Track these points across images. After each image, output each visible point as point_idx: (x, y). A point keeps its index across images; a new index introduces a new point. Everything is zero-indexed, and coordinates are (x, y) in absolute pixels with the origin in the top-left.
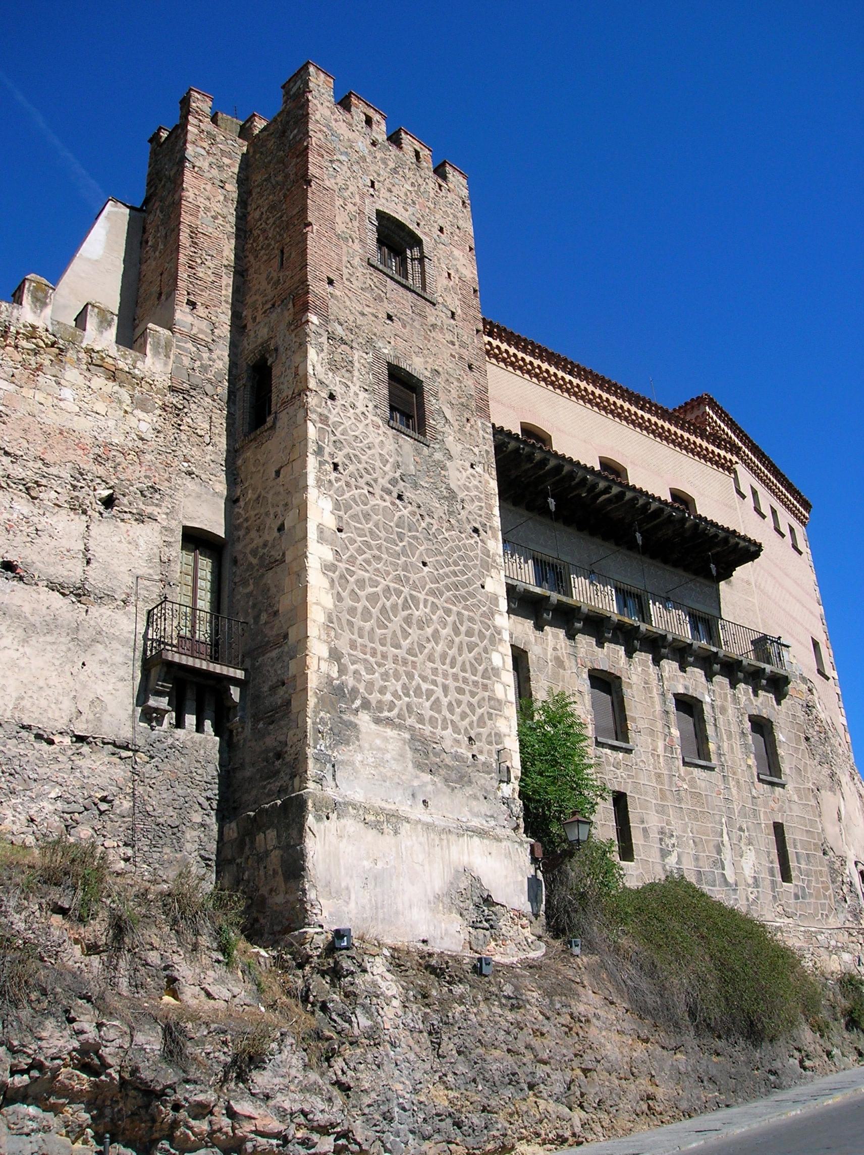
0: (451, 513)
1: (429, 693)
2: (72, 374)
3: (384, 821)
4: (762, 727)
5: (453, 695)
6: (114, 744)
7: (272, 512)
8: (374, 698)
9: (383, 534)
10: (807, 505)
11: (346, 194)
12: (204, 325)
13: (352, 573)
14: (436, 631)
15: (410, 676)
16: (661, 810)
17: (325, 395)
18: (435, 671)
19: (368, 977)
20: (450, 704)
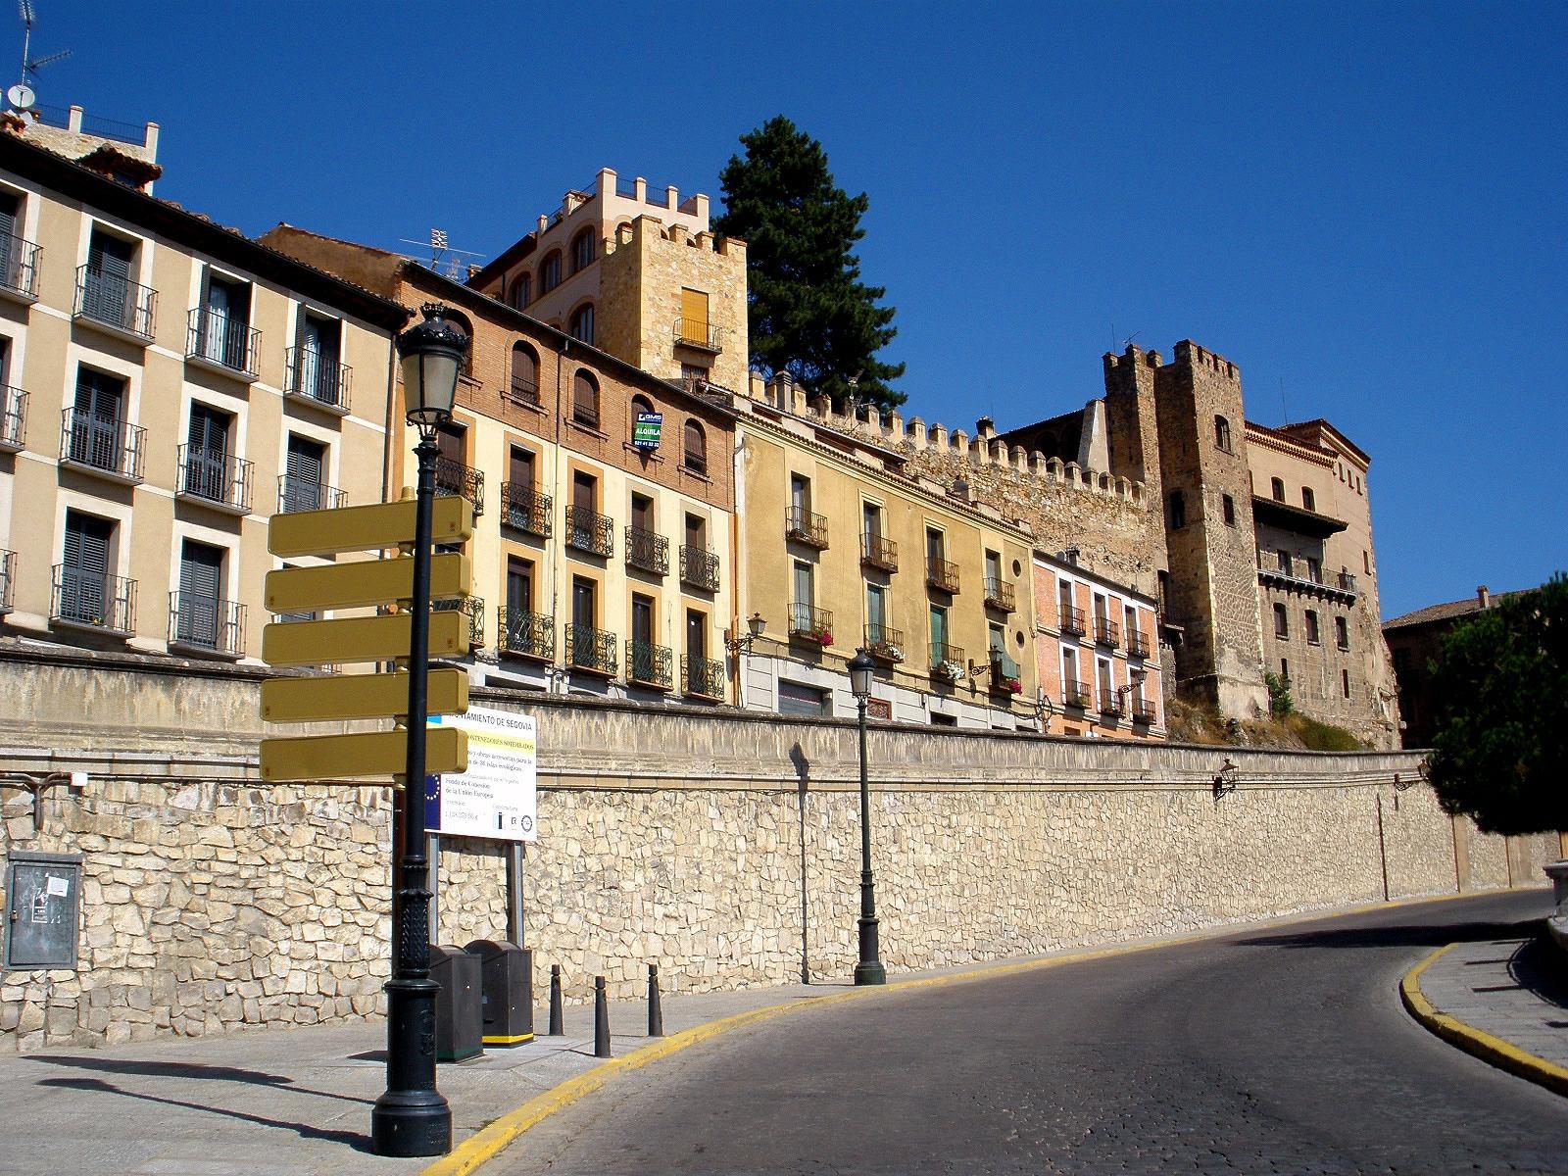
3: (1234, 682)
4: (1341, 622)
10: (1367, 460)
16: (1299, 666)
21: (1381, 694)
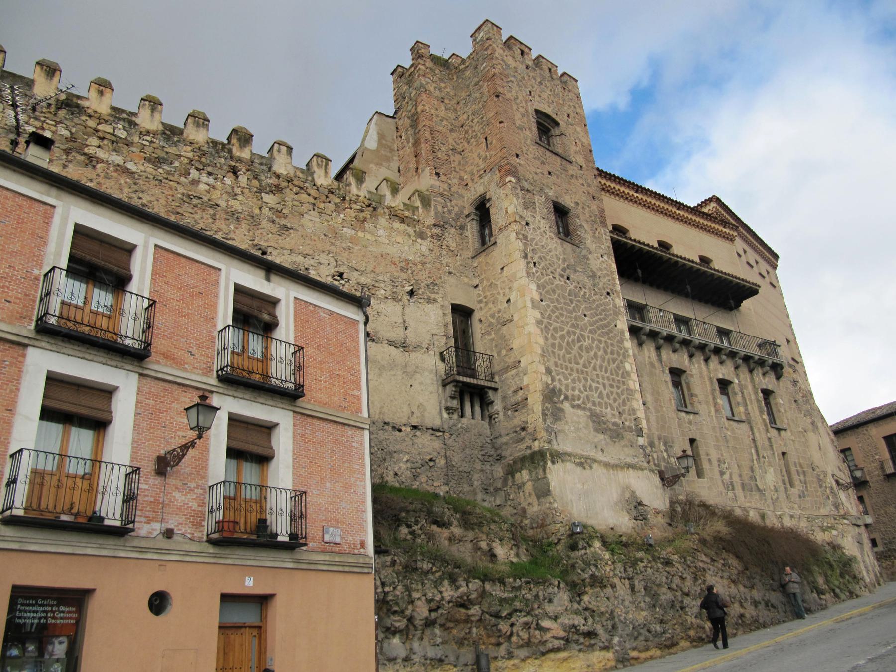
0: (594, 285)
1: (597, 388)
2: (383, 221)
3: (584, 463)
5: (608, 389)
6: (432, 429)
7: (501, 292)
8: (570, 393)
9: (562, 301)
11: (518, 101)
12: (445, 186)
13: (550, 324)
14: (596, 354)
15: (586, 380)
16: (718, 448)
17: (524, 223)
18: (598, 376)
19: (592, 549)
20: (607, 394)
21: (837, 482)
